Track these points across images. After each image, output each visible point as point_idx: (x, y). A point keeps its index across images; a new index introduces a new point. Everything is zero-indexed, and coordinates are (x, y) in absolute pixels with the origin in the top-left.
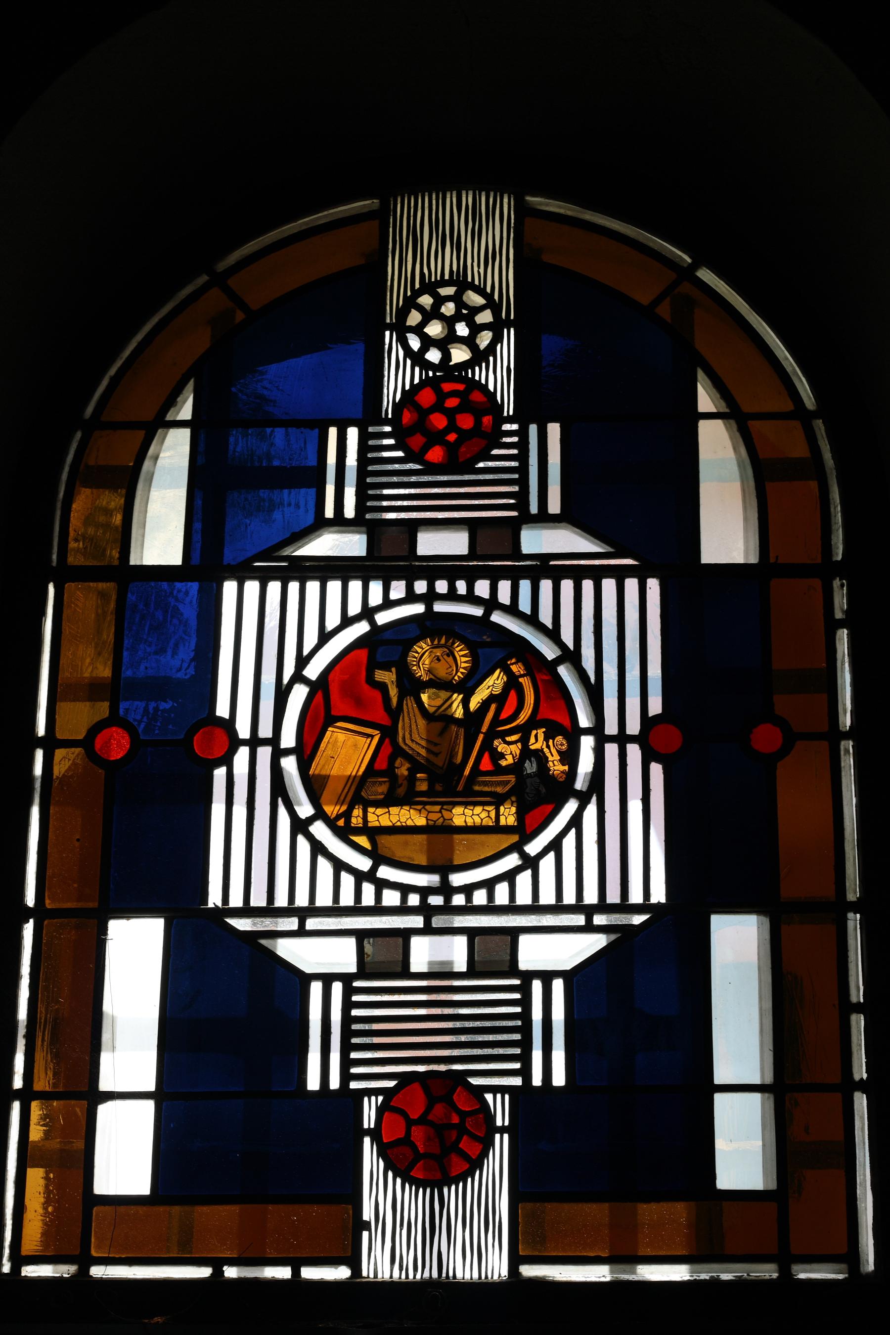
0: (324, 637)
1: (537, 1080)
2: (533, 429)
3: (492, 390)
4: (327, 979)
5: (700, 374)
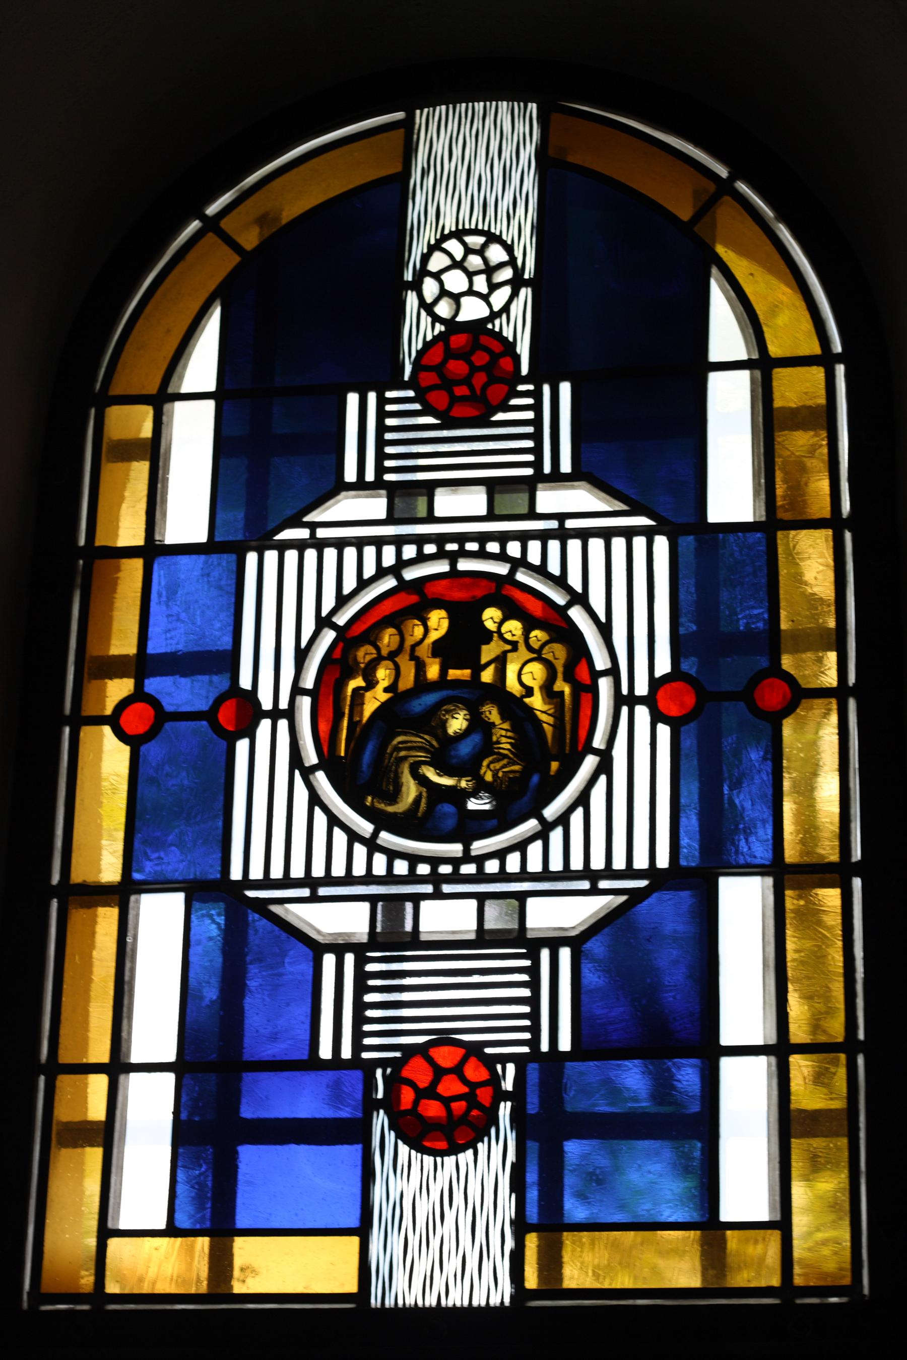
0: (583, 800)
1: (372, 397)
2: (546, 389)
3: (494, 418)
4: (339, 949)
5: (714, 271)
